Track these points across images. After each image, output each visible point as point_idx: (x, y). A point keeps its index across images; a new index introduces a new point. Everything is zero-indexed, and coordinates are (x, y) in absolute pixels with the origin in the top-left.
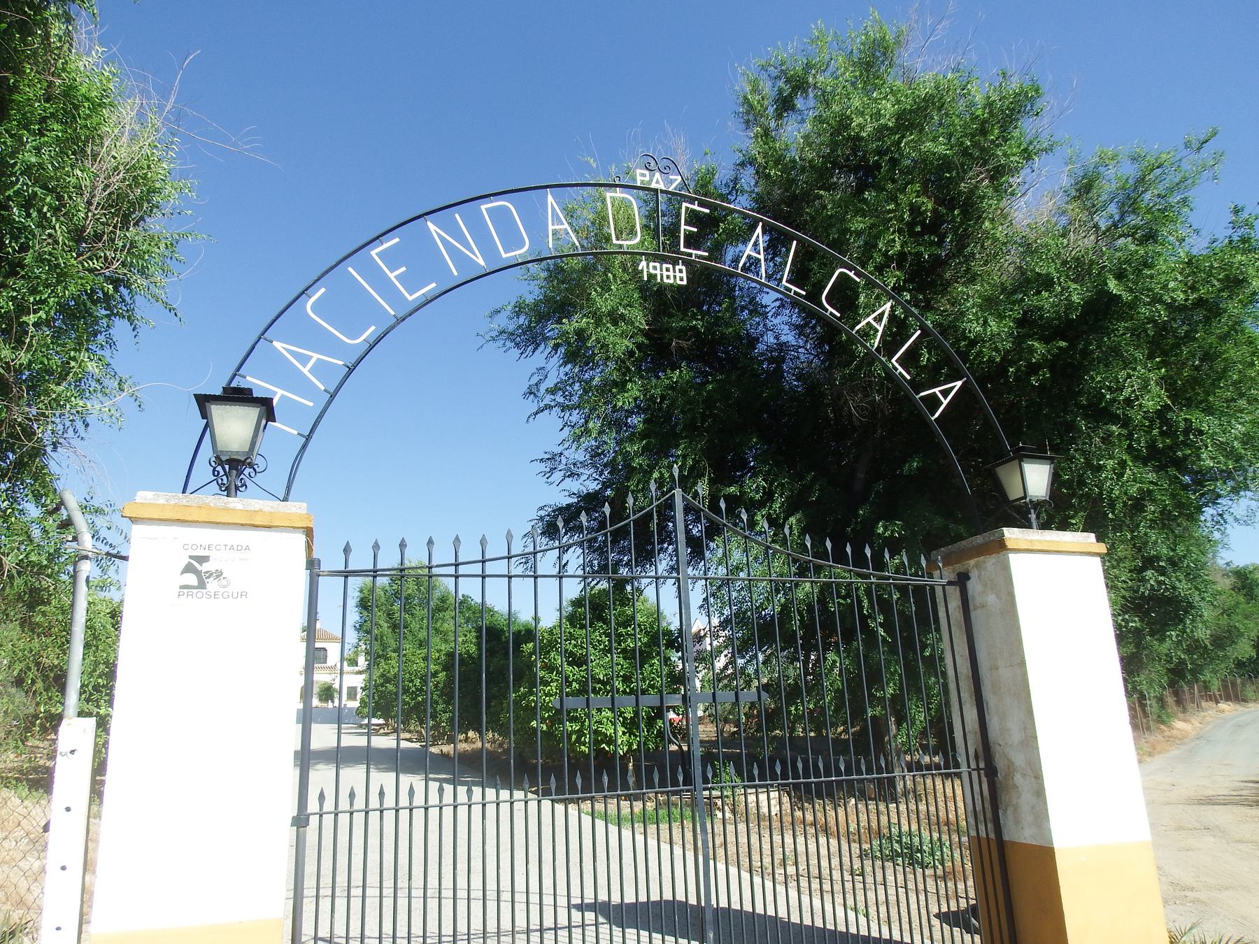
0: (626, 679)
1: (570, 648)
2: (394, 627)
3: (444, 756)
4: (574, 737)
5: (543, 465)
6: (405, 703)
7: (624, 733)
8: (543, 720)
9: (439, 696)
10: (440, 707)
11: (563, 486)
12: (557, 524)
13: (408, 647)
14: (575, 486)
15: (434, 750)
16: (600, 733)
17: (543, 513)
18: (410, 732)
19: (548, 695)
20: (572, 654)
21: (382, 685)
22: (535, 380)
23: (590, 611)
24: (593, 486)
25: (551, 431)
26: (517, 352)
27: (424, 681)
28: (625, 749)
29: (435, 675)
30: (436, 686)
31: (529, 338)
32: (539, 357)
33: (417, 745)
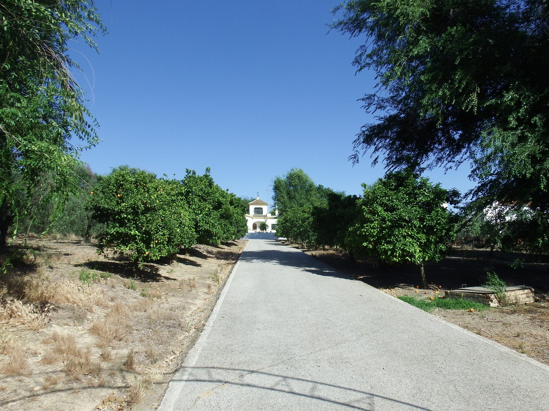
0: (422, 220)
1: (385, 201)
2: (290, 198)
3: (313, 256)
4: (389, 253)
5: (364, 102)
6: (295, 231)
7: (420, 251)
8: (370, 242)
9: (311, 228)
10: (311, 233)
11: (375, 114)
12: (371, 136)
13: (296, 207)
14: (382, 113)
15: (309, 253)
16: (405, 251)
17: (364, 129)
18: (298, 244)
19: (372, 228)
20: (386, 205)
21: (284, 223)
22: (359, 53)
23: (396, 182)
24: (394, 112)
25: (369, 80)
26: (348, 34)
27: (303, 222)
28: (421, 260)
29: (308, 218)
30: (309, 224)
31: (356, 25)
32: (364, 35)
33: (299, 251)
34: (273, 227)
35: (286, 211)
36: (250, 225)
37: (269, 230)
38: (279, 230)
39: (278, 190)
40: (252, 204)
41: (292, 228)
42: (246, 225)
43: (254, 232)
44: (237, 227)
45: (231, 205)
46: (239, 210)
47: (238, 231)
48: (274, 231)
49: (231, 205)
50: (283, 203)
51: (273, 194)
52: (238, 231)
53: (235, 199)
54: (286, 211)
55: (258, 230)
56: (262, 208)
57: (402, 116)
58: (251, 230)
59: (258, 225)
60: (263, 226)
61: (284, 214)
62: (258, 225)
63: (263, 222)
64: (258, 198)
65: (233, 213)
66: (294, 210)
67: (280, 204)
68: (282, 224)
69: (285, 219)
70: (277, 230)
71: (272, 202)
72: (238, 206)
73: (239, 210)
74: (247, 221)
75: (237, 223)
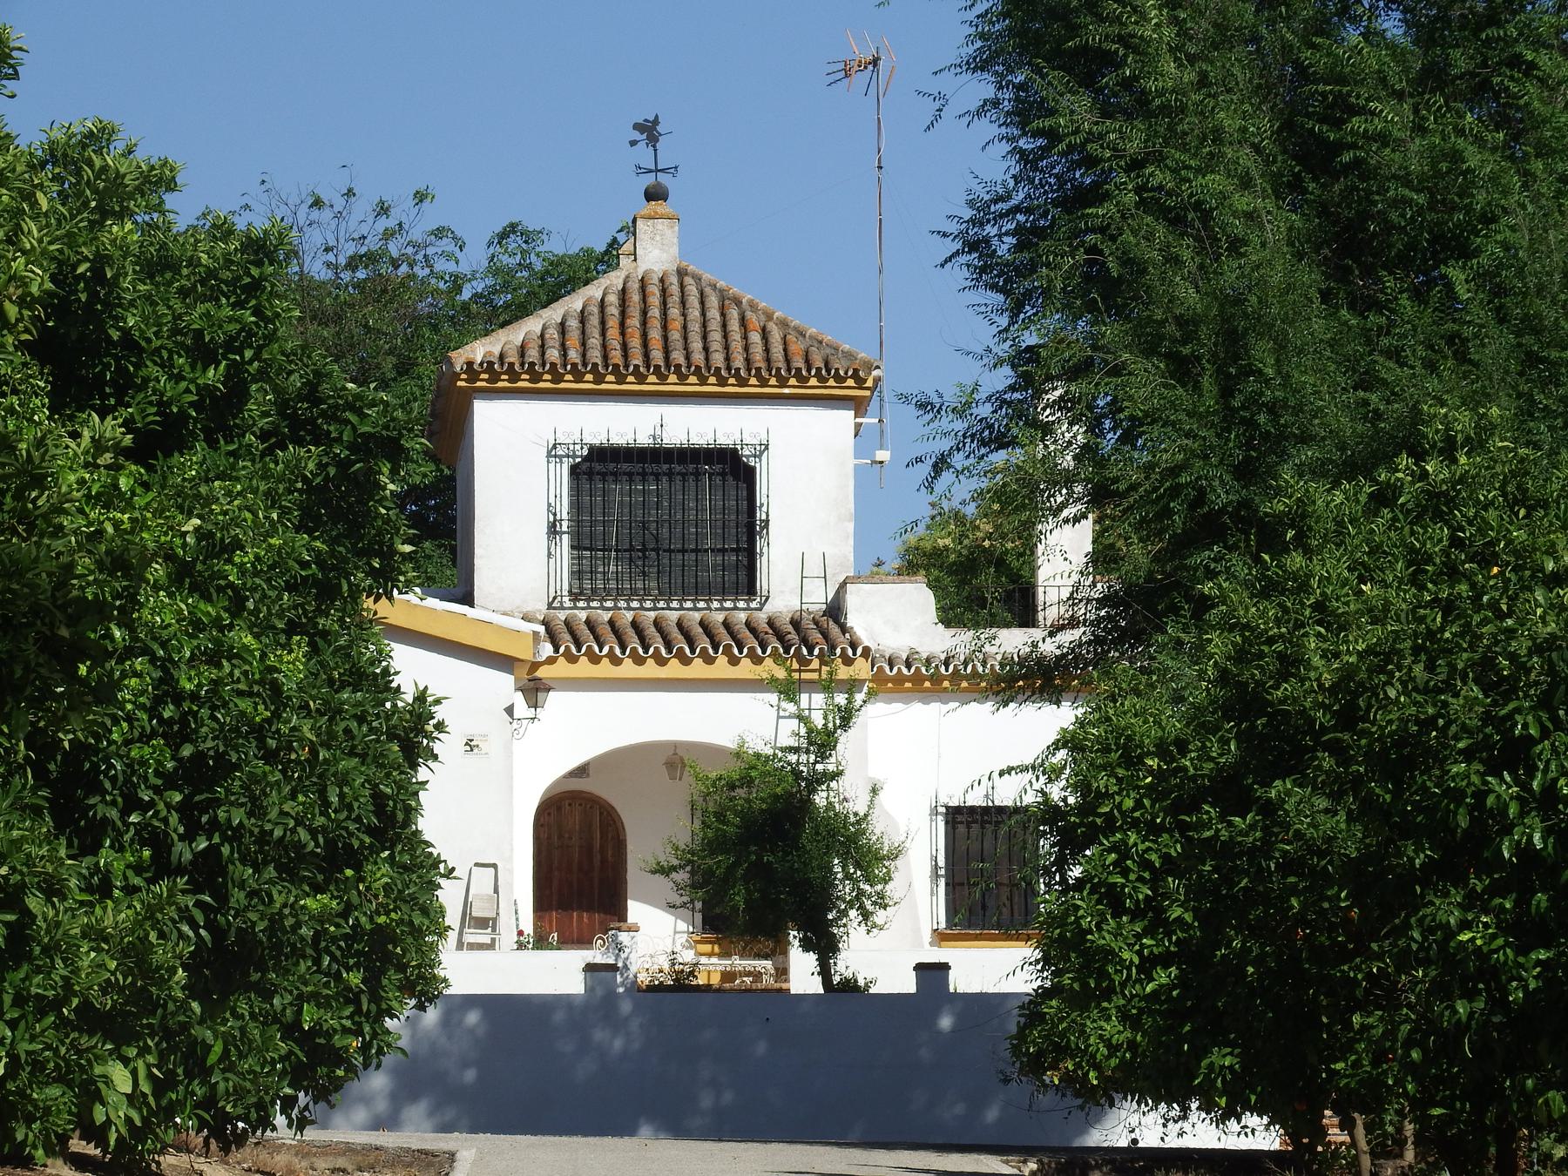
2: (1353, 250)
6: (1461, 972)
21: (1231, 791)
34: (988, 862)
35: (1269, 536)
36: (478, 811)
37: (890, 944)
38: (1123, 942)
39: (1087, 67)
40: (525, 378)
41: (1385, 893)
42: (393, 821)
43: (559, 973)
44: (208, 873)
45: (72, 396)
46: (242, 504)
47: (227, 966)
48: (1000, 969)
49: (72, 396)
50: (1217, 354)
51: (974, 157)
52: (227, 966)
53: (159, 265)
54: (1269, 536)
55: (657, 936)
56: (731, 469)
57: (147, 853)
58: (495, 957)
59: (656, 832)
60: (775, 855)
61: (1227, 580)
62: (656, 832)
63: (750, 769)
64: (656, 251)
65: (123, 564)
66: (1436, 504)
67: (1146, 382)
68: (1179, 799)
69: (1240, 701)
70: (1063, 947)
71: (953, 340)
72: (220, 413)
73: (242, 504)
74: (413, 732)
75: (200, 776)
